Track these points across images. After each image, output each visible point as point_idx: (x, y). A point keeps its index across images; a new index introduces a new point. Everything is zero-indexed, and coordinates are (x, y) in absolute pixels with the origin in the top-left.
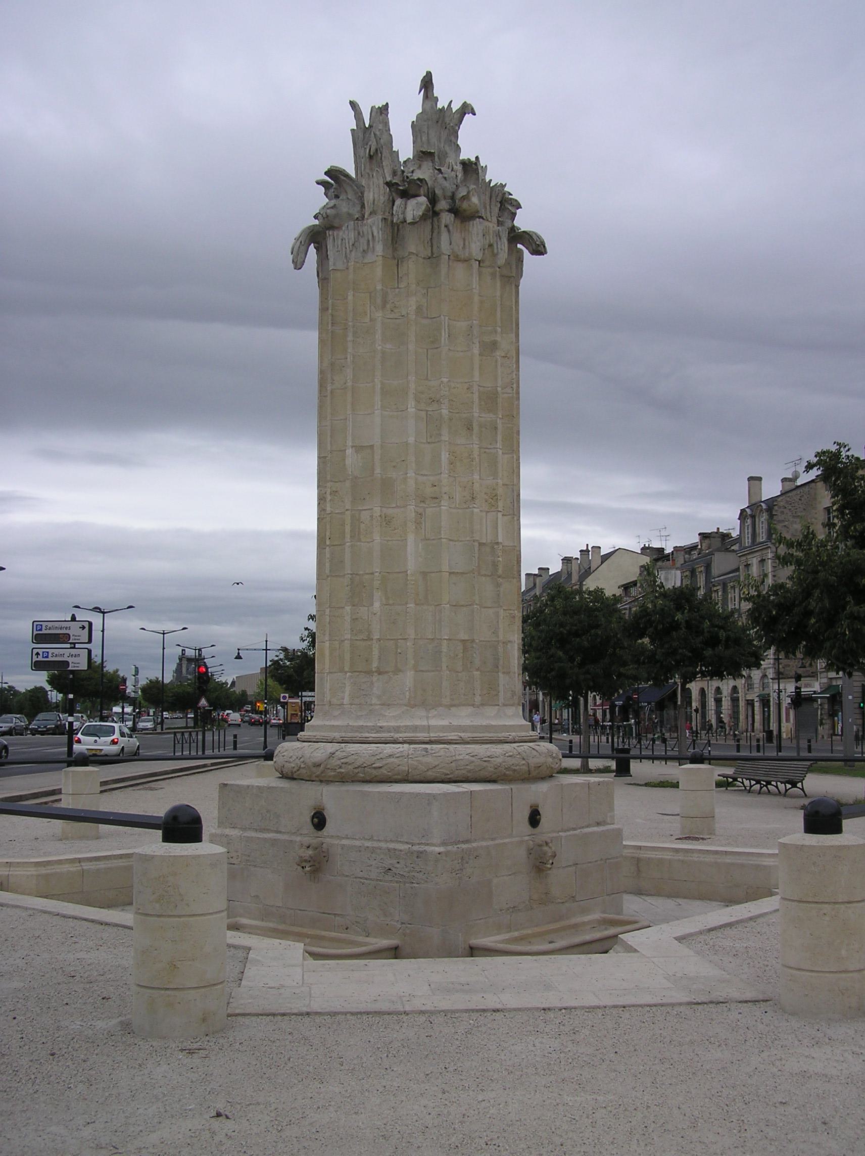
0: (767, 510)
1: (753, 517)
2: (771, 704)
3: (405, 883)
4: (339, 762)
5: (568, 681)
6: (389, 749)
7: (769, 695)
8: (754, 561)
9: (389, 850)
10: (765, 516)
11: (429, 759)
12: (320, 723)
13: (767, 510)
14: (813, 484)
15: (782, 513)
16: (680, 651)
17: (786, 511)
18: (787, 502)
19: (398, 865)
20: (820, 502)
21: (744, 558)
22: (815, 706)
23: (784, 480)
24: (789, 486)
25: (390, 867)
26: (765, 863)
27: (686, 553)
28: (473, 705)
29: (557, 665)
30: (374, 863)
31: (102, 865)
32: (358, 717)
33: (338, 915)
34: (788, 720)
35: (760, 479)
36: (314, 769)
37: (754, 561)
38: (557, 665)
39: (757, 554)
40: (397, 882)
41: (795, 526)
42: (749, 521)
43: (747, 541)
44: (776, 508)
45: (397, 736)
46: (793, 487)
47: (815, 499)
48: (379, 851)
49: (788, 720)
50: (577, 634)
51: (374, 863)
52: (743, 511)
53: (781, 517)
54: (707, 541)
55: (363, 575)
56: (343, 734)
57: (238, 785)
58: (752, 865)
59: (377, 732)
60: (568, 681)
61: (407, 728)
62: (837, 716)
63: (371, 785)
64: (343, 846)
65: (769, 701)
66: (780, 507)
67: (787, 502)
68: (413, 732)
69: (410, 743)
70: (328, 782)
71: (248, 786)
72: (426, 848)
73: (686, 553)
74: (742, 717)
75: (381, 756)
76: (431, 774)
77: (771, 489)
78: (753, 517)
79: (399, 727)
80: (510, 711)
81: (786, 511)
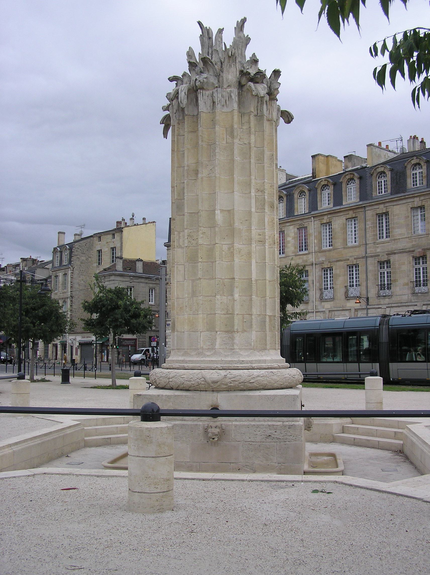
0: (69, 249)
1: (61, 252)
2: (67, 346)
3: (280, 442)
4: (229, 380)
5: (31, 333)
6: (256, 372)
7: (66, 341)
8: (61, 274)
9: (269, 426)
10: (68, 252)
11: (275, 377)
12: (175, 359)
13: (69, 249)
14: (92, 238)
15: (77, 251)
16: (120, 320)
17: (79, 250)
18: (79, 246)
19: (276, 433)
20: (95, 247)
21: (55, 272)
22: (93, 347)
23: (75, 235)
24: (78, 238)
25: (270, 434)
26: (329, 423)
27: (13, 268)
28: (275, 349)
29: (25, 325)
30: (258, 433)
31: (31, 443)
32: (226, 356)
33: (233, 463)
34: (76, 354)
35: (64, 233)
36: (212, 385)
37: (61, 274)
38: (25, 325)
39: (63, 271)
40: (274, 442)
41: (82, 258)
42: (58, 254)
43: (57, 264)
44: (74, 248)
45: (254, 365)
46: (80, 238)
47: (93, 246)
48: (262, 427)
49: (76, 354)
50: (34, 309)
51: (258, 433)
52: (55, 249)
53: (76, 253)
54: (25, 262)
55: (224, 279)
56: (222, 365)
57: (150, 395)
58: (323, 424)
59: (241, 364)
60: (31, 333)
61: (257, 361)
62: (104, 352)
63: (254, 391)
64: (236, 426)
65: (66, 344)
66: (76, 248)
67: (79, 246)
68: (259, 363)
69: (260, 369)
70: (218, 391)
71: (159, 396)
72: (293, 423)
73: (13, 268)
74: (50, 352)
75: (254, 376)
76: (276, 385)
77: (69, 239)
78: (61, 252)
79: (252, 361)
80: (272, 352)
81: (79, 250)
